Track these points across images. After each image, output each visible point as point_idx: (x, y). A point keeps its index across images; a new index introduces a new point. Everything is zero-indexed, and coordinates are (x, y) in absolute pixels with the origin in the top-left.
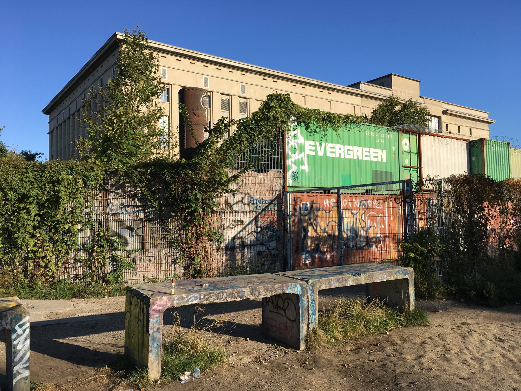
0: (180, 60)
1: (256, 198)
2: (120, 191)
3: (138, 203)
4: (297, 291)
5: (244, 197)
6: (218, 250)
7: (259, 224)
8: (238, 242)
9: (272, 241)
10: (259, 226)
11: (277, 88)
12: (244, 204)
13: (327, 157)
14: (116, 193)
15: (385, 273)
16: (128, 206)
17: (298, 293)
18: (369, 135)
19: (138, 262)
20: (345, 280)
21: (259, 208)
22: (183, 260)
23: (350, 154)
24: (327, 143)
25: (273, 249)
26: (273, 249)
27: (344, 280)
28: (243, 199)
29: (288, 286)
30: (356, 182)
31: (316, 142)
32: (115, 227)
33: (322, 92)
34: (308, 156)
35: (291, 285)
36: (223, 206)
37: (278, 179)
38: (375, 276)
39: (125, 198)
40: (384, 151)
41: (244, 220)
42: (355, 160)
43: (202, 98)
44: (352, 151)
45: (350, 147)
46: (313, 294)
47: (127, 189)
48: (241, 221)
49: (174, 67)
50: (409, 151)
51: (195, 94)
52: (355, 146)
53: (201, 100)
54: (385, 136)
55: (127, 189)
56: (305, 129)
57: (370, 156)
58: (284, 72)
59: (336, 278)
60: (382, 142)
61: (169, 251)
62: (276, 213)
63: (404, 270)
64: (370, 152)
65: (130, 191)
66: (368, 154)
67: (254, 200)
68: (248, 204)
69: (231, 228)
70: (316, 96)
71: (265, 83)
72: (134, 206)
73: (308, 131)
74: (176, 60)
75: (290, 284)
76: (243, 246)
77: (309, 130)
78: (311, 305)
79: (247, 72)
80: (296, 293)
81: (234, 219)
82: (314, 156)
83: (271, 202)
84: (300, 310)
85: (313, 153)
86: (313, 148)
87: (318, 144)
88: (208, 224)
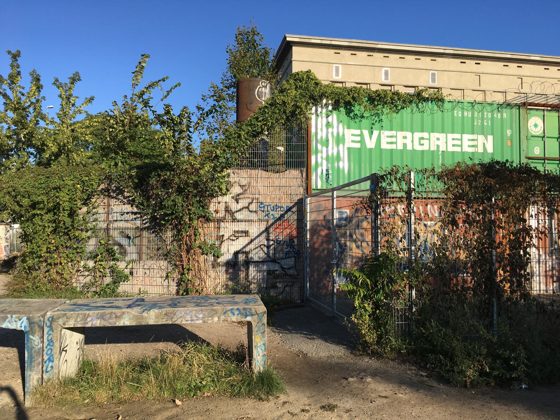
0: (356, 54)
1: (267, 204)
2: (120, 197)
3: (135, 210)
4: (21, 327)
5: (251, 203)
6: (215, 265)
7: (272, 237)
8: (241, 257)
9: (288, 258)
10: (271, 238)
11: (480, 71)
12: (251, 211)
13: (381, 150)
14: (117, 199)
15: (202, 310)
16: (128, 213)
17: (23, 329)
18: (460, 115)
19: (135, 274)
20: (116, 317)
21: (272, 217)
22: (176, 275)
23: (423, 145)
24: (382, 131)
25: (290, 268)
26: (290, 268)
27: (114, 316)
28: (249, 205)
29: (7, 318)
30: (338, 182)
31: (363, 131)
32: (115, 234)
33: (548, 69)
34: (349, 149)
35: (12, 317)
36: (221, 215)
37: (299, 181)
38: (179, 314)
39: (124, 204)
40: (490, 138)
41: (250, 231)
42: (433, 151)
43: (257, 90)
44: (427, 139)
45: (425, 135)
46: (50, 332)
47: (126, 194)
48: (246, 233)
49: (331, 62)
50: (542, 135)
51: (249, 85)
52: (433, 132)
53: (256, 92)
54: (492, 115)
55: (126, 194)
56: (346, 114)
57: (461, 146)
58: (490, 50)
59: (98, 313)
60: (485, 124)
61: (163, 264)
62: (295, 223)
63: (244, 309)
64: (461, 140)
65: (129, 197)
66: (459, 143)
67: (264, 207)
68: (256, 212)
69: (233, 240)
70: (539, 75)
71: (464, 67)
72: (132, 213)
73: (350, 117)
74: (351, 54)
75: (9, 316)
76: (248, 263)
77: (352, 115)
78: (46, 347)
79: (439, 57)
80: (19, 328)
81: (236, 229)
82: (360, 150)
83: (289, 210)
84: (26, 352)
85: (358, 146)
86: (358, 139)
87: (366, 133)
88: (202, 234)
